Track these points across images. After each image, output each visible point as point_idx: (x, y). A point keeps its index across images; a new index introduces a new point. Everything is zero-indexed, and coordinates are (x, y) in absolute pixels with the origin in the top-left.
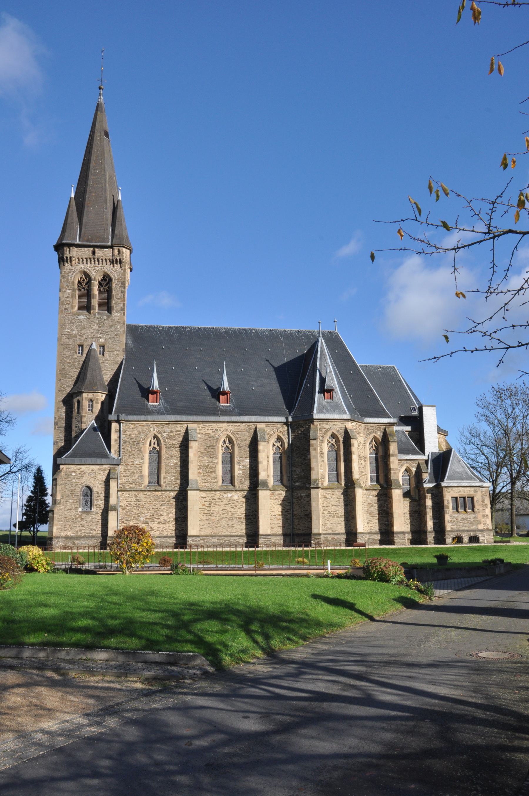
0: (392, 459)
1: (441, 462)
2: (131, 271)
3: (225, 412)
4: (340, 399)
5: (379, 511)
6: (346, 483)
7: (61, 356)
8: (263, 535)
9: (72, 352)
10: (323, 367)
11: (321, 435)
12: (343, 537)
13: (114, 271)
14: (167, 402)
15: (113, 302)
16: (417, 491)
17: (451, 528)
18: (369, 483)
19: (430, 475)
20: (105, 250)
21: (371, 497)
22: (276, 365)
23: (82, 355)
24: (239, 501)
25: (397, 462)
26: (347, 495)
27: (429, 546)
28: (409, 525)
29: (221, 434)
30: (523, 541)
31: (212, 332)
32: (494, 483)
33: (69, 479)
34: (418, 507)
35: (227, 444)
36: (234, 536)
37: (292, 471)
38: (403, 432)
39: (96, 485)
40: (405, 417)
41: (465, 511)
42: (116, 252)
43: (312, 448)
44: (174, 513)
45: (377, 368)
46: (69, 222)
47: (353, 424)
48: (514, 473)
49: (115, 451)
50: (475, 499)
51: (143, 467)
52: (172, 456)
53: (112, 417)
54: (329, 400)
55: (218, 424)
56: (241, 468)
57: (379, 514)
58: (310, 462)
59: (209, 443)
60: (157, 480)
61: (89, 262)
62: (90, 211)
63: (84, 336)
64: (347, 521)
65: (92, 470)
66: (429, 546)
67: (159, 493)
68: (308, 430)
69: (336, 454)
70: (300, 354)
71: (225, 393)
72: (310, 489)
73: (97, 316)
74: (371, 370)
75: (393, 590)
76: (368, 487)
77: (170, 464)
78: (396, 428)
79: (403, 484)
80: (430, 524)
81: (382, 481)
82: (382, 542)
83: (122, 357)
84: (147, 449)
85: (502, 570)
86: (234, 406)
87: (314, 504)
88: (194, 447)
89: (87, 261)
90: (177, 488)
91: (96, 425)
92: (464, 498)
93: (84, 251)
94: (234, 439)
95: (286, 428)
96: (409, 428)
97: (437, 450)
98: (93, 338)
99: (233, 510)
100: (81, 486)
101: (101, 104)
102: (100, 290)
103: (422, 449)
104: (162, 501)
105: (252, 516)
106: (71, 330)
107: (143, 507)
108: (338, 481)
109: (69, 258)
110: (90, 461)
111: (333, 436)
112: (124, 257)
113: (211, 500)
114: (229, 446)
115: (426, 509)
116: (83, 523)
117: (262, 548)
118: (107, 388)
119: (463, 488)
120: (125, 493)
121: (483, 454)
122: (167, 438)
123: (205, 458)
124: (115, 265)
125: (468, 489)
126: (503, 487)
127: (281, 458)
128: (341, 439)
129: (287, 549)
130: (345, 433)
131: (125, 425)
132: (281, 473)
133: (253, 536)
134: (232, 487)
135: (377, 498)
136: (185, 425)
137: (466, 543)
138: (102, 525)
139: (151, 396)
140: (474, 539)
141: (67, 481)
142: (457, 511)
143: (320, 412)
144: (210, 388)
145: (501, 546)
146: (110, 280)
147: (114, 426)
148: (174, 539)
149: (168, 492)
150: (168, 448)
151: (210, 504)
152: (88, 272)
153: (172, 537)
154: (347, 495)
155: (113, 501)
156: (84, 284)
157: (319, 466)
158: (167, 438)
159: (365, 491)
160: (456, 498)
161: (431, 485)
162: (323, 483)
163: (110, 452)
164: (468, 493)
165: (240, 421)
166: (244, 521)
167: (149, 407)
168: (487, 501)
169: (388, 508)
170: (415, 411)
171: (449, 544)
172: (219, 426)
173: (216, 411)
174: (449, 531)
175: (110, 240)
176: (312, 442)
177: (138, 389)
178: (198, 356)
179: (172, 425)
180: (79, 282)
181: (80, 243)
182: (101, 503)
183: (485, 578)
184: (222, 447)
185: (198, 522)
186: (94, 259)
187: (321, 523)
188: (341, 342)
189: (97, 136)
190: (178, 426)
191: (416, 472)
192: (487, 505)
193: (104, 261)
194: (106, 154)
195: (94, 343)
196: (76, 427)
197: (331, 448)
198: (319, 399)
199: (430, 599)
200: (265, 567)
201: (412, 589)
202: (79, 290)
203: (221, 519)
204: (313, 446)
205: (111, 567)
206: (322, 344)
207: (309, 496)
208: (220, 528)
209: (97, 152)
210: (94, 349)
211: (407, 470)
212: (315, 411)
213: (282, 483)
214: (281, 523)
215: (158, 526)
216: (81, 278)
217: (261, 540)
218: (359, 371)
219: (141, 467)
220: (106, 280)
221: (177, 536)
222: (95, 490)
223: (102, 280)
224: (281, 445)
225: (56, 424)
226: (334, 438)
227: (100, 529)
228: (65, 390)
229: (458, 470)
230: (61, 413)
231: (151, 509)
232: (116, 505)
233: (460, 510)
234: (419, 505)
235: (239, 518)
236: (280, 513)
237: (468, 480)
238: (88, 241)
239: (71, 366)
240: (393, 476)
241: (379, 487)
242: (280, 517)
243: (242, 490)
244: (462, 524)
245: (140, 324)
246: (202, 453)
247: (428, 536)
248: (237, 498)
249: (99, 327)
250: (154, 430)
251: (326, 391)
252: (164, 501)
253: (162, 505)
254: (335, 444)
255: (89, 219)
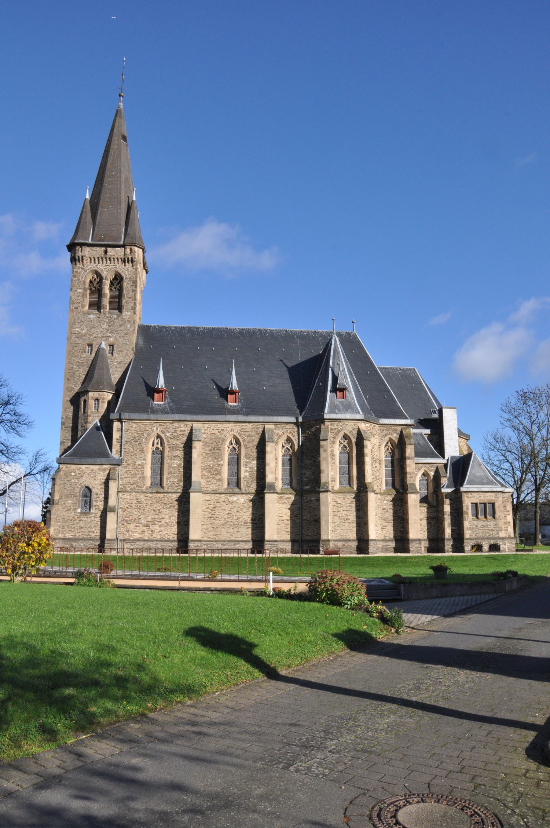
0: (408, 462)
1: (460, 467)
2: (147, 273)
3: (233, 412)
4: (353, 399)
5: (394, 516)
6: (358, 486)
7: (70, 354)
8: (269, 541)
9: (81, 351)
10: (336, 365)
11: (332, 436)
12: (355, 544)
13: (126, 270)
14: (172, 401)
15: (124, 301)
16: (435, 496)
17: (470, 535)
18: (384, 487)
19: (448, 479)
20: (117, 249)
21: (385, 502)
22: (290, 365)
23: (91, 354)
24: (246, 505)
25: (413, 465)
26: (359, 500)
27: (446, 554)
28: (426, 532)
29: (227, 435)
30: (546, 550)
31: (226, 332)
32: (518, 490)
33: (69, 479)
34: (436, 513)
35: (233, 445)
36: (239, 541)
37: (302, 474)
38: (421, 435)
39: (96, 486)
40: (425, 420)
41: (486, 517)
42: (128, 251)
43: (322, 450)
44: (176, 516)
45: (396, 369)
46: (82, 222)
47: (367, 425)
48: (538, 480)
49: (117, 451)
50: (497, 505)
51: (145, 468)
52: (175, 457)
53: (114, 416)
54: (342, 400)
55: (224, 424)
56: (248, 470)
57: (394, 520)
58: (320, 465)
59: (215, 444)
60: (159, 481)
61: (101, 262)
62: (103, 211)
63: (94, 336)
64: (359, 526)
65: (92, 470)
66: (446, 554)
67: (161, 495)
68: (319, 430)
69: (349, 456)
70: (315, 354)
71: (233, 392)
72: (319, 492)
73: (107, 315)
74: (390, 372)
75: (340, 619)
76: (382, 491)
77: (173, 465)
78: (413, 431)
79: (420, 489)
80: (448, 532)
81: (398, 485)
82: (396, 550)
83: (132, 357)
84: (149, 449)
85: (515, 585)
86: (242, 405)
87: (323, 509)
88: (198, 447)
89: (99, 260)
90: (180, 490)
91: (99, 424)
92: (485, 504)
93: (96, 251)
94: (241, 440)
95: (296, 429)
96: (428, 431)
97: (457, 454)
98: (103, 337)
99: (238, 514)
100: (80, 487)
101: (121, 110)
102: (111, 290)
103: (441, 452)
104: (164, 504)
105: (259, 520)
106: (81, 329)
107: (144, 510)
108: (350, 485)
109: (80, 258)
110: (89, 460)
111: (346, 437)
112: (136, 256)
113: (216, 503)
114: (236, 447)
115: (443, 515)
116: (82, 524)
117: (267, 554)
118: (115, 388)
119: (484, 493)
120: (126, 494)
121: (508, 461)
122: (170, 438)
123: (210, 459)
124: (127, 264)
125: (489, 494)
126: (528, 494)
127: (290, 460)
128: (354, 440)
129: (298, 556)
130: (357, 434)
131: (127, 424)
132: (291, 476)
133: (258, 542)
134: (237, 490)
135: (392, 503)
136: (189, 425)
137: (486, 552)
138: (101, 527)
139: (156, 395)
140: (494, 547)
141: (66, 481)
142: (477, 517)
143: (332, 411)
144: (219, 387)
145: (522, 555)
146: (122, 279)
147: (116, 425)
148: (176, 543)
149: (171, 494)
150: (171, 449)
151: (214, 507)
152: (99, 271)
153: (248, 541)
154: (359, 500)
155: (112, 502)
156: (95, 284)
157: (330, 469)
158: (170, 438)
159: (379, 496)
160: (476, 504)
161: (449, 490)
162: (333, 487)
163: (111, 451)
164: (489, 498)
165: (248, 420)
166: (250, 526)
167: (154, 406)
168: (509, 508)
169: (403, 514)
170: (436, 413)
171: (468, 553)
172: (225, 426)
173: (223, 411)
174: (468, 539)
175: (123, 240)
176: (322, 443)
177: (144, 388)
178: (209, 356)
179: (176, 425)
180: (91, 282)
181: (92, 242)
182: (101, 505)
183: (491, 597)
184: (228, 447)
185: (200, 526)
186: (106, 258)
187: (330, 528)
188: (359, 342)
189: (115, 139)
190: (182, 425)
191: (434, 476)
192: (509, 511)
193: (116, 260)
194: (123, 157)
195: (103, 342)
196: (82, 427)
197: (343, 450)
198: (331, 397)
199: (397, 632)
200: (219, 577)
201: (373, 617)
202: (91, 289)
203: (226, 523)
204: (323, 447)
205: (67, 572)
206: (336, 341)
207: (318, 500)
208: (225, 533)
209: (114, 155)
210: (103, 349)
211: (425, 474)
212: (326, 410)
213: (292, 487)
214: (289, 529)
215: (159, 529)
216: (93, 277)
217: (267, 546)
218: (377, 371)
219: (143, 468)
220: (118, 279)
221: (179, 541)
222: (94, 490)
223: (113, 279)
224: (291, 447)
225: (63, 424)
226: (346, 439)
227: (99, 532)
228: (72, 389)
229: (478, 474)
230: (69, 412)
231: (152, 512)
232: (115, 506)
233: (480, 517)
234: (437, 511)
235: (245, 523)
236: (289, 518)
237: (489, 485)
238: (100, 240)
239: (80, 365)
240: (409, 480)
241: (394, 492)
242: (289, 522)
243: (249, 493)
244: (482, 531)
245: (153, 325)
246: (207, 454)
247: (446, 544)
248: (243, 502)
249: (109, 326)
250: (157, 430)
251: (338, 390)
252: (166, 504)
253: (163, 508)
254: (347, 445)
255: (105, 221)
